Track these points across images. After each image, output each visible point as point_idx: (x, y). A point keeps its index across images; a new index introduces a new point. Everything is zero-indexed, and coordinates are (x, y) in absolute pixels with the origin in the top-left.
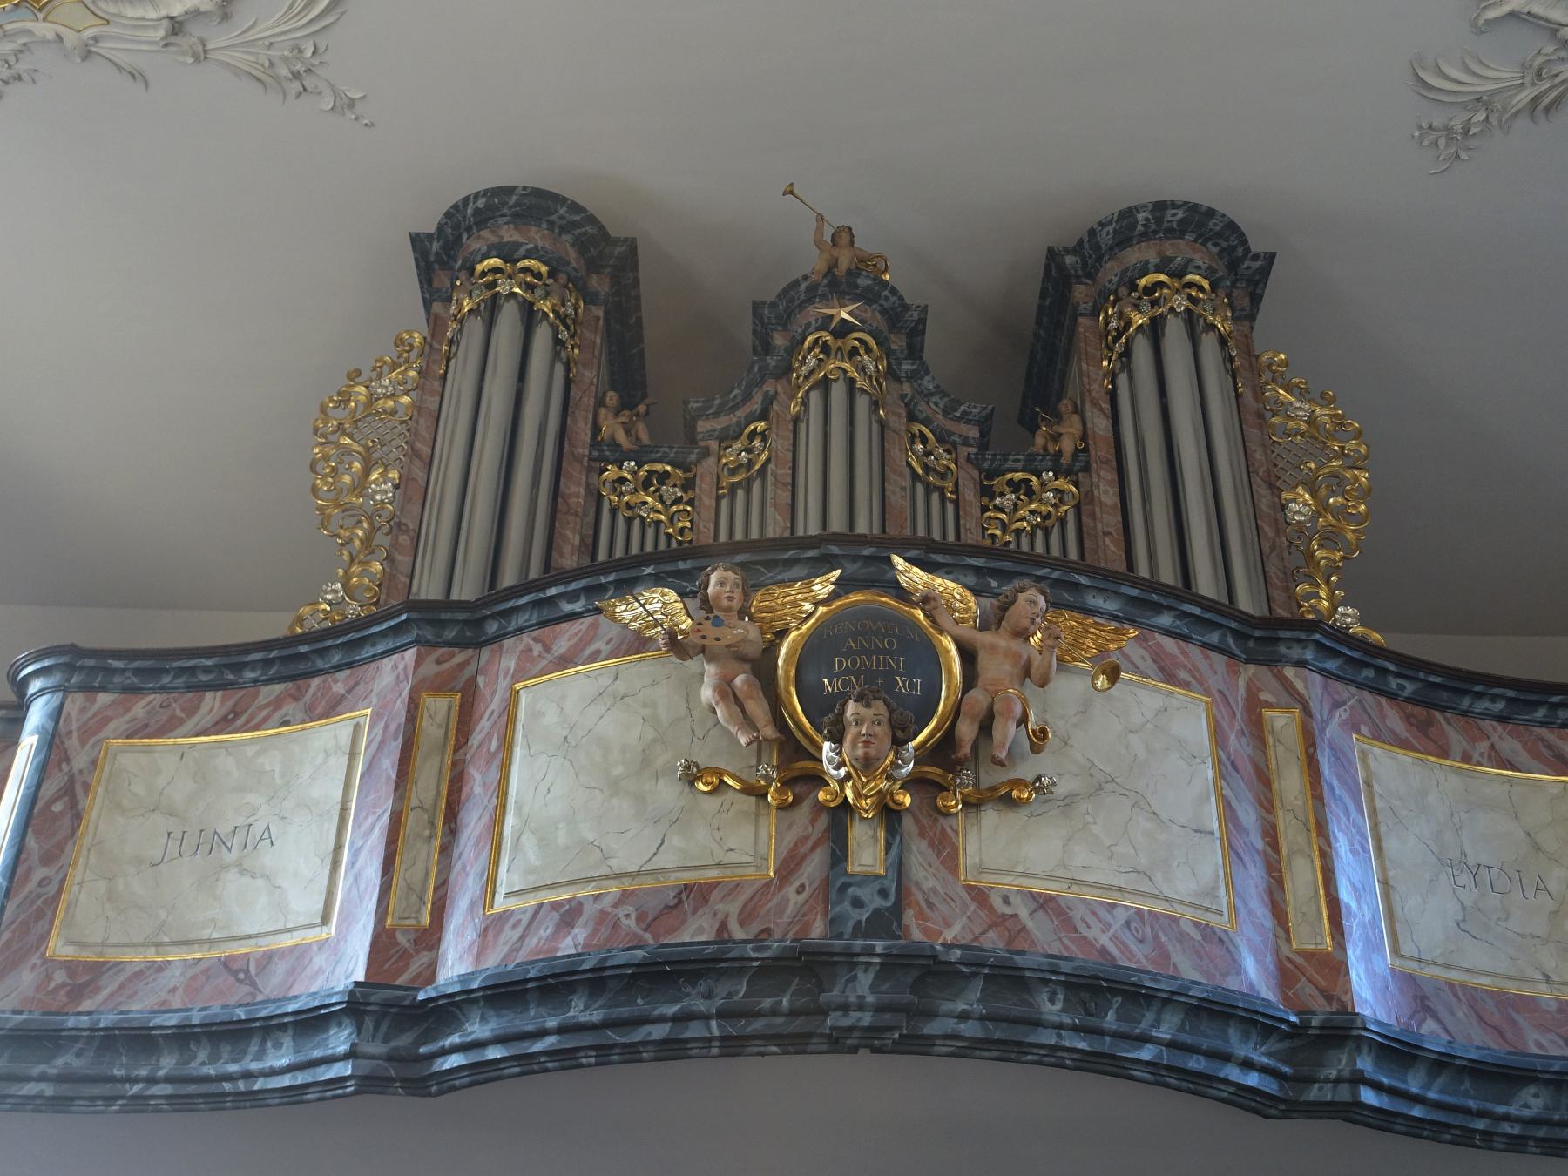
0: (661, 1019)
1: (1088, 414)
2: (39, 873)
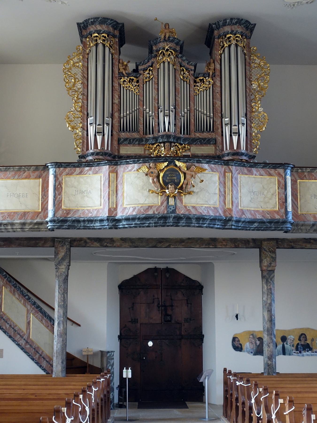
0: (147, 223)
1: (216, 64)
2: (59, 197)
